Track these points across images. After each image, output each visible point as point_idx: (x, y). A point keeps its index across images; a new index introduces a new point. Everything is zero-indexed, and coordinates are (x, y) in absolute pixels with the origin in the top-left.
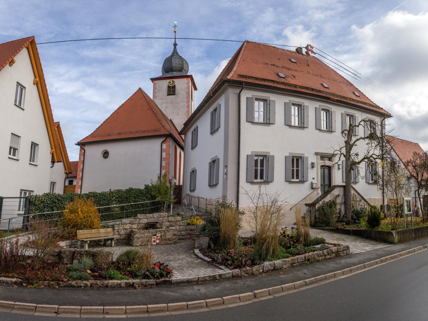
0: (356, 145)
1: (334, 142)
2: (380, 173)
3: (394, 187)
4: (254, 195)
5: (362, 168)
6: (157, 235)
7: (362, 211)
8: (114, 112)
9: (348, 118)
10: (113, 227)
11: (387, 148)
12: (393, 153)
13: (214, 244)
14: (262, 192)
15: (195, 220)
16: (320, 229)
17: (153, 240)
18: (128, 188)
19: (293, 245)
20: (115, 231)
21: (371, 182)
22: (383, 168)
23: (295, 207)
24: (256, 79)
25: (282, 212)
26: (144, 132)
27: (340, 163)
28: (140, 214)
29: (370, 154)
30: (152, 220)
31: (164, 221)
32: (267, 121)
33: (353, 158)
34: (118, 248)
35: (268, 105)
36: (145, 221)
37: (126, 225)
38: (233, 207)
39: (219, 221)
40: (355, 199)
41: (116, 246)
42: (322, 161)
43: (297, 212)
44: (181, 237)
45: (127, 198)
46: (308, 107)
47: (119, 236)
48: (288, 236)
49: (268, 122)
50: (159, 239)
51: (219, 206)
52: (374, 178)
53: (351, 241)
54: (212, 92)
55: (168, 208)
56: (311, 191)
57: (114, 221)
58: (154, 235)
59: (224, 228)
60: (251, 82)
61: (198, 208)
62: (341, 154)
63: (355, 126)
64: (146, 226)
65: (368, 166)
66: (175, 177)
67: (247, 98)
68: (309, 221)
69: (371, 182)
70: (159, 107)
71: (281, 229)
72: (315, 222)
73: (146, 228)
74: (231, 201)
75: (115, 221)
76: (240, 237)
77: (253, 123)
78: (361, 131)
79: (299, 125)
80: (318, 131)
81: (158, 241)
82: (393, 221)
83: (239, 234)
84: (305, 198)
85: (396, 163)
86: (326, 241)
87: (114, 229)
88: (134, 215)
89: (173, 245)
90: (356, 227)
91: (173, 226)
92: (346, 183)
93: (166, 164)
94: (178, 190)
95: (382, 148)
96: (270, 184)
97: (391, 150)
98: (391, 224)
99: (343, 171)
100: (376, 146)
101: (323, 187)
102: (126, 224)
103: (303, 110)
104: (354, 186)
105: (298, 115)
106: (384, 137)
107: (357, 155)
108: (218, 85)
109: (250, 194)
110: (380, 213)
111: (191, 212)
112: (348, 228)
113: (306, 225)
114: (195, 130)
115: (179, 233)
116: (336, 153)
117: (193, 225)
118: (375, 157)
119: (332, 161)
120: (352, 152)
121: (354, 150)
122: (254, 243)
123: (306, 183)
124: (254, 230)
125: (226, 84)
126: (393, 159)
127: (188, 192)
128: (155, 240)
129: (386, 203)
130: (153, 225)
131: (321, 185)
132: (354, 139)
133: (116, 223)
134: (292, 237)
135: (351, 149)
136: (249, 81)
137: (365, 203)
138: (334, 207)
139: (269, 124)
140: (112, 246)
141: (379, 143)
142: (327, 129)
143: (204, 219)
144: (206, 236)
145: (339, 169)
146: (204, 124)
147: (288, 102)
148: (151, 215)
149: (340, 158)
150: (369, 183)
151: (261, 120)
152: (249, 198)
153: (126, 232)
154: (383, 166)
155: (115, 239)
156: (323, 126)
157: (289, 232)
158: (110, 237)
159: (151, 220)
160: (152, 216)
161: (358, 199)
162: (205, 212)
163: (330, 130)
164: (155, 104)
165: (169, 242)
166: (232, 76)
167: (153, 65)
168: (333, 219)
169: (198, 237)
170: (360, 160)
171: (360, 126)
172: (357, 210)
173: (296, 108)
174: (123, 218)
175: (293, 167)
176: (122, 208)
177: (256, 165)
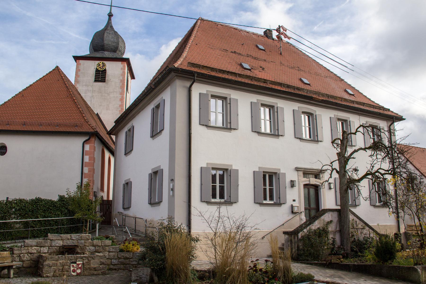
0: (353, 158)
1: (323, 155)
2: (392, 193)
3: (414, 209)
4: (211, 218)
5: (364, 187)
6: (78, 263)
7: (366, 241)
8: (18, 94)
9: (339, 124)
10: (11, 250)
11: (400, 160)
12: (410, 166)
13: (158, 277)
14: (222, 214)
15: (131, 245)
16: (304, 263)
17: (72, 269)
18: (34, 198)
19: (268, 282)
20: (15, 256)
21: (378, 204)
22: (395, 186)
23: (269, 235)
24: (213, 69)
25: (251, 240)
26: (59, 125)
27: (331, 180)
28: (51, 233)
29: (375, 169)
30: (70, 243)
31: (87, 244)
32: (227, 125)
33: (350, 174)
34: (19, 280)
35: (228, 105)
36: (60, 243)
37: (32, 247)
38: (183, 231)
39: (164, 248)
40: (355, 226)
41: (16, 277)
42: (305, 179)
43: (273, 241)
44: (112, 267)
45: (33, 211)
46: (282, 109)
47: (21, 263)
48: (261, 270)
49: (228, 126)
50: (80, 268)
51: (163, 230)
52: (382, 199)
53: (351, 279)
54: (154, 83)
55: (93, 229)
56: (292, 216)
57: (13, 241)
58: (72, 263)
59: (171, 257)
60: (206, 73)
61: (135, 231)
62: (333, 169)
63: (351, 133)
64: (61, 250)
65: (373, 184)
66: (102, 189)
67: (200, 93)
68: (289, 253)
69: (378, 204)
70: (83, 95)
71: (250, 262)
72: (298, 255)
73: (62, 253)
74: (179, 225)
75: (15, 242)
76: (193, 269)
77: (208, 126)
78: (359, 140)
79: (271, 131)
80: (298, 141)
81: (79, 271)
82: (416, 253)
83: (193, 266)
84: (283, 225)
85: (416, 178)
86: (314, 279)
87: (13, 253)
88: (44, 234)
89: (101, 276)
90: (359, 262)
91: (99, 252)
92: (341, 206)
93: (89, 171)
94: (107, 206)
95: (392, 161)
96: (234, 205)
97: (407, 162)
98: (413, 258)
99: (336, 192)
100: (383, 159)
101: (307, 211)
102: (31, 246)
103: (276, 113)
104: (353, 210)
105: (270, 119)
106: (395, 146)
107: (356, 170)
108: (162, 74)
109: (206, 216)
110: (394, 244)
111: (126, 235)
112: (346, 262)
113: (285, 259)
114: (129, 130)
115: (109, 262)
116: (324, 168)
117: (128, 251)
118: (383, 172)
119: (320, 179)
120: (348, 167)
121: (351, 165)
122: (214, 278)
123: (283, 206)
124: (213, 261)
125: (173, 74)
126: (411, 173)
127: (122, 210)
128: (75, 269)
129: (402, 230)
130: (71, 248)
131: (306, 209)
132: (350, 150)
133: (16, 244)
134: (266, 272)
135: (346, 162)
136: (202, 72)
137: (371, 230)
138: (326, 237)
139: (230, 129)
140: (9, 277)
141: (388, 154)
142: (310, 137)
143: (142, 245)
144: (147, 267)
145: (330, 188)
146: (142, 123)
147: (256, 101)
148: (68, 236)
149: (331, 175)
150: (375, 206)
151: (220, 124)
152: (205, 221)
153: (32, 257)
154: (395, 184)
155: (14, 267)
156: (306, 134)
157: (261, 265)
158: (7, 264)
159: (69, 242)
160: (69, 237)
161: (360, 226)
162: (145, 237)
163: (314, 138)
164: (77, 90)
165: (96, 273)
166: (181, 64)
167: (77, 36)
168: (324, 251)
169: (136, 267)
170: (360, 176)
171: (357, 133)
172: (358, 240)
173: (267, 110)
174: (27, 238)
175: (265, 184)
176: (26, 225)
177: (214, 181)
